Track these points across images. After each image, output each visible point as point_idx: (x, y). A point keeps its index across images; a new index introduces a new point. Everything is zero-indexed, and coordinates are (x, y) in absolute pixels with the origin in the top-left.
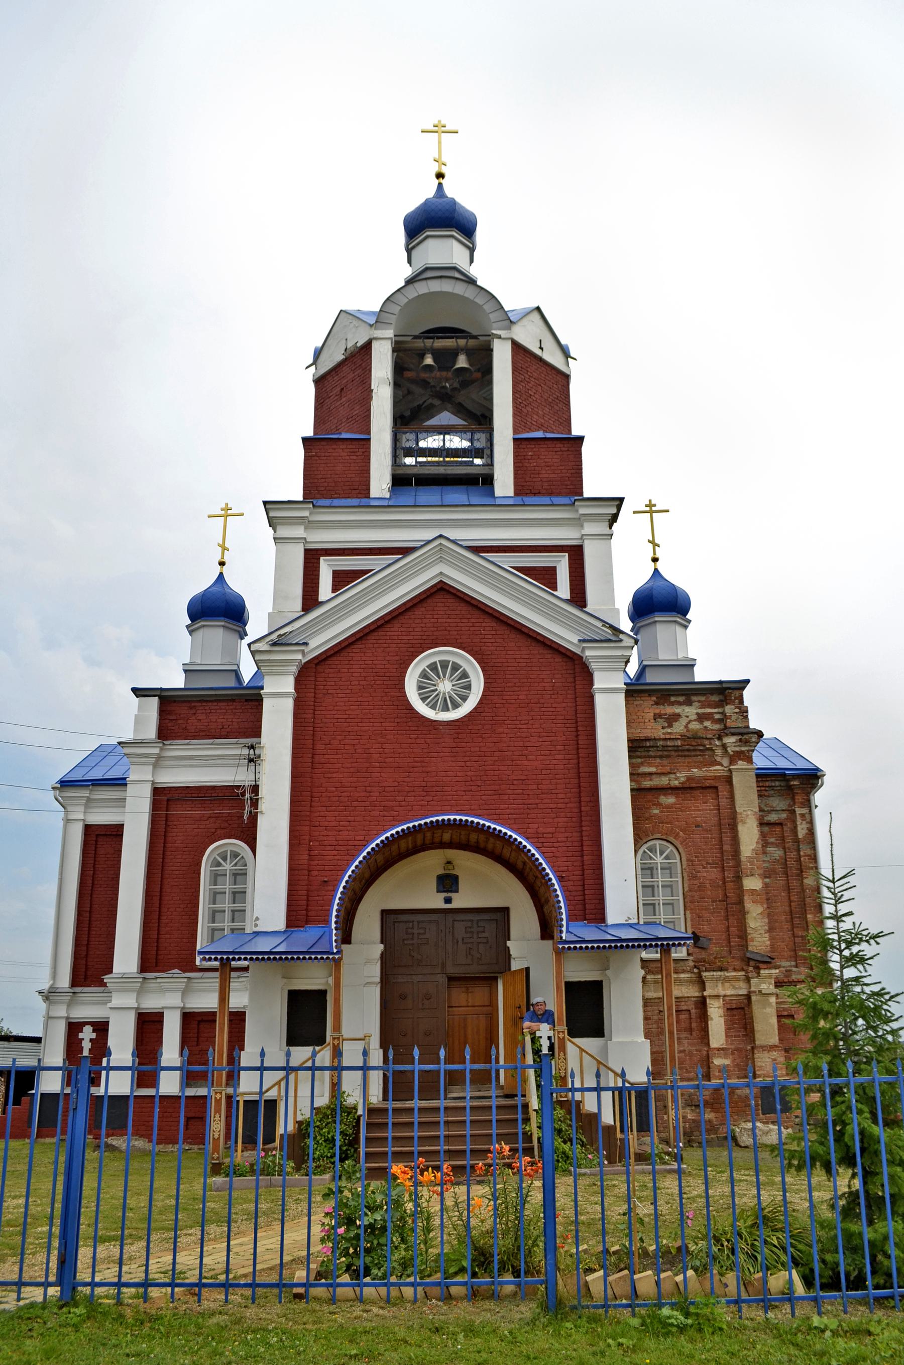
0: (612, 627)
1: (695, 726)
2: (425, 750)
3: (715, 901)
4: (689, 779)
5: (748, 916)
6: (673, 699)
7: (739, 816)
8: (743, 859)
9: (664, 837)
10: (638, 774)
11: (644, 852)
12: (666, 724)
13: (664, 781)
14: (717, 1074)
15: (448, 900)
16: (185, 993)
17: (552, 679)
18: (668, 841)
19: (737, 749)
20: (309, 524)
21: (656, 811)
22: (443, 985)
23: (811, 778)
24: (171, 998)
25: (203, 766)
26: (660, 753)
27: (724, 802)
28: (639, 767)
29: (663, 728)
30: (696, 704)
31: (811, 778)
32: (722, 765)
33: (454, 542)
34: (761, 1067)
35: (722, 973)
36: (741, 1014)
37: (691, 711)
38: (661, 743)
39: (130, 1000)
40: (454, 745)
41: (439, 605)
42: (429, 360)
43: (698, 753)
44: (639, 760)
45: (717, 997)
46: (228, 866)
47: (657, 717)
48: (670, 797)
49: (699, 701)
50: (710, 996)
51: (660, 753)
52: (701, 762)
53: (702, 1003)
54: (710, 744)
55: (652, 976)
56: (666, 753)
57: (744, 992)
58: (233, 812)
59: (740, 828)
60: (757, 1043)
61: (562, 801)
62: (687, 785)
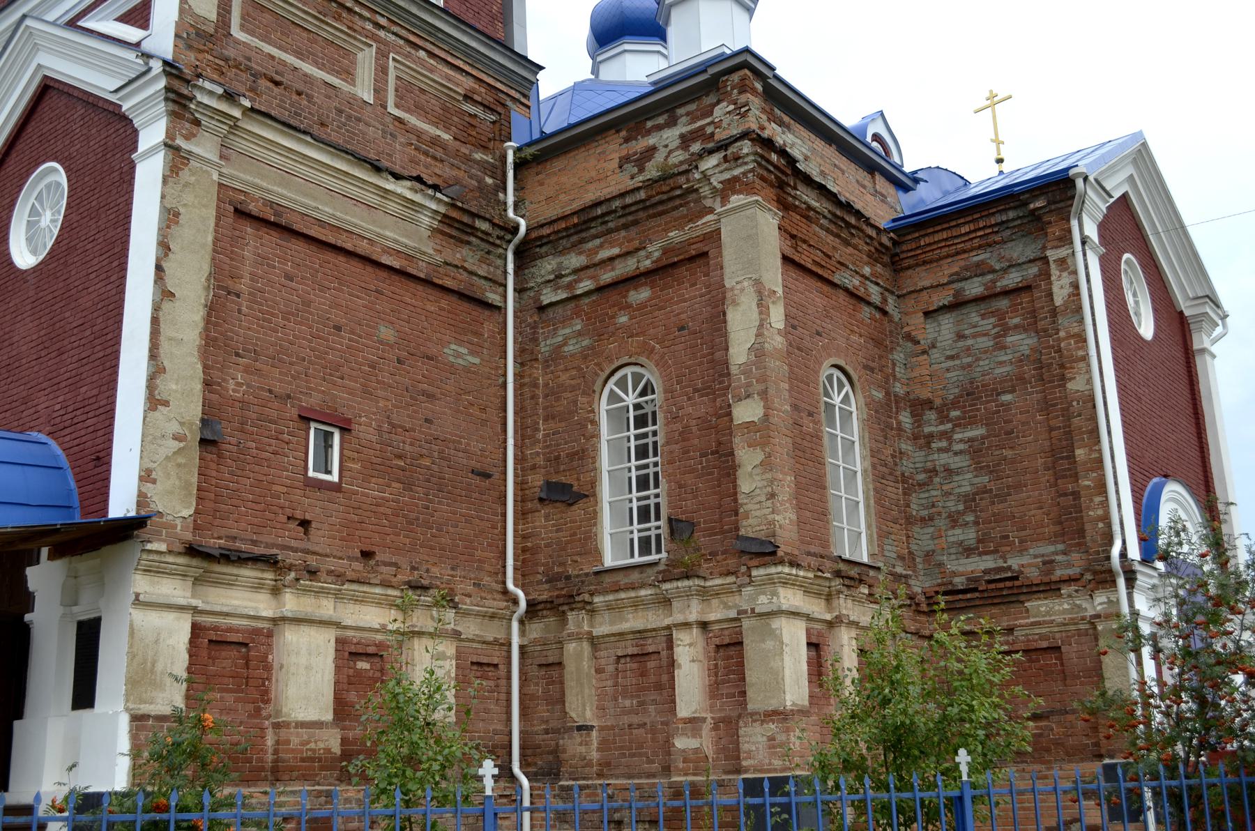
4: (666, 251)
5: (740, 473)
6: (649, 124)
7: (729, 295)
8: (734, 370)
10: (595, 265)
11: (612, 390)
13: (629, 266)
14: (681, 765)
19: (727, 176)
21: (623, 319)
28: (597, 253)
34: (749, 752)
36: (729, 653)
37: (671, 136)
43: (678, 202)
44: (597, 242)
45: (686, 625)
48: (642, 289)
49: (688, 114)
50: (675, 625)
51: (623, 221)
54: (688, 181)
56: (630, 218)
57: (732, 614)
60: (750, 707)
62: (664, 262)
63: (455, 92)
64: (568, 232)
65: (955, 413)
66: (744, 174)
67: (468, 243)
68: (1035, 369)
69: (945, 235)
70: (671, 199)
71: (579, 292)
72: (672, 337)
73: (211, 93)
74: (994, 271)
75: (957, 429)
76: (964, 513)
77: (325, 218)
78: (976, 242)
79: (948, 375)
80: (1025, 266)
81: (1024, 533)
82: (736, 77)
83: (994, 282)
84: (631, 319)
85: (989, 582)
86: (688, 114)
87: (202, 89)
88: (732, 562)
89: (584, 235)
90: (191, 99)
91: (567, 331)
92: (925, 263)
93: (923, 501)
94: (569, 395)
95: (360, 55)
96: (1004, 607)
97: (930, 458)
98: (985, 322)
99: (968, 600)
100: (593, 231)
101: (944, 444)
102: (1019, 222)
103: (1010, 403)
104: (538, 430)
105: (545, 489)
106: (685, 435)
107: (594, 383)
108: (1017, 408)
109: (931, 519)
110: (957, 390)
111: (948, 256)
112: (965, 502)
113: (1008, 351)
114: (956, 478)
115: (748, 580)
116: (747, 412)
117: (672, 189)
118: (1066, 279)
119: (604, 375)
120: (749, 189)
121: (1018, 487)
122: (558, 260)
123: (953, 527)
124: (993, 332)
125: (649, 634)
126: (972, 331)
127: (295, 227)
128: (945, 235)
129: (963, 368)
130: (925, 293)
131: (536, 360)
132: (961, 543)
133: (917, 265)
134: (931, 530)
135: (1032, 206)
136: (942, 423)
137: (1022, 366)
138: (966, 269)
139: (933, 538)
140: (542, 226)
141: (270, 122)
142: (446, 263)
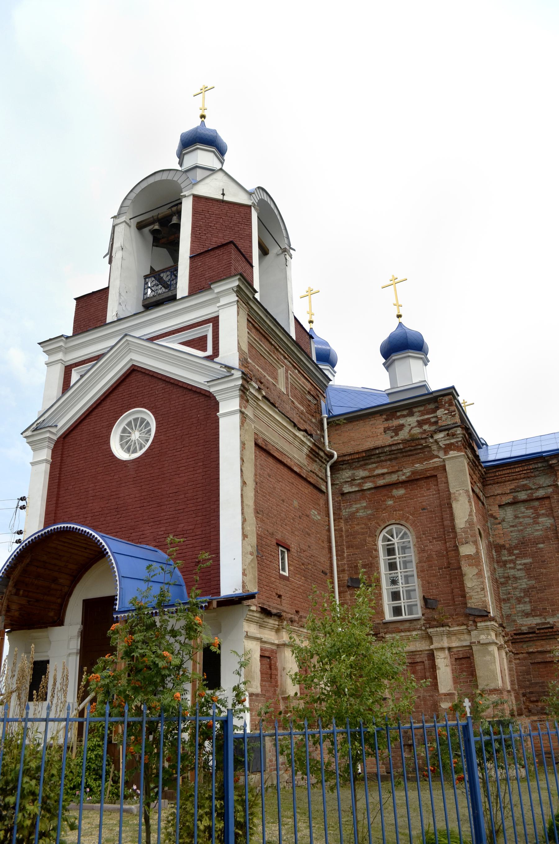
0: (226, 367)
1: (416, 431)
2: (118, 483)
3: (442, 569)
4: (413, 473)
6: (398, 414)
7: (452, 496)
8: (458, 531)
9: (397, 522)
10: (374, 476)
12: (393, 434)
13: (394, 478)
17: (197, 415)
18: (402, 525)
19: (448, 442)
26: (389, 457)
28: (374, 471)
29: (392, 437)
30: (417, 414)
32: (439, 457)
33: (139, 338)
35: (444, 629)
36: (465, 662)
37: (412, 420)
38: (387, 449)
40: (136, 475)
41: (132, 381)
43: (419, 451)
44: (374, 465)
45: (442, 649)
49: (419, 411)
50: (436, 649)
51: (389, 457)
52: (422, 458)
53: (431, 656)
54: (426, 442)
55: (390, 635)
56: (393, 456)
57: (467, 643)
59: (454, 505)
61: (200, 503)
62: (413, 478)
63: (304, 388)
64: (359, 460)
65: (516, 552)
66: (457, 442)
67: (316, 461)
68: (553, 534)
69: (508, 471)
70: (415, 450)
71: (365, 488)
72: (419, 512)
73: (254, 387)
74: (531, 489)
75: (518, 559)
76: (524, 597)
77: (279, 448)
78: (522, 476)
79: (512, 534)
80: (546, 488)
81: (553, 607)
82: (447, 398)
83: (532, 494)
84: (394, 502)
85: (538, 629)
86: (419, 411)
87: (252, 385)
88: (461, 619)
89: (367, 461)
90: (247, 390)
91: (358, 506)
92: (498, 483)
93: (504, 591)
94: (361, 536)
95: (279, 371)
96: (547, 641)
97: (506, 571)
98: (528, 511)
99: (530, 637)
100: (372, 460)
101: (512, 565)
102: (543, 468)
103: (543, 548)
104: (344, 552)
105: (350, 581)
106: (429, 559)
107: (375, 531)
108: (546, 550)
109: (508, 599)
110: (516, 541)
111: (509, 481)
112: (524, 592)
113: (540, 525)
114: (519, 581)
115: (475, 628)
116: (466, 550)
117: (417, 445)
119: (380, 528)
120: (458, 449)
121: (550, 586)
122: (353, 472)
123: (519, 604)
124: (532, 516)
125: (417, 653)
126: (522, 515)
127: (271, 452)
128: (508, 471)
129: (519, 531)
130: (499, 497)
131: (341, 518)
132: (523, 611)
133: (494, 484)
134: (509, 605)
135: (551, 462)
136: (510, 556)
137: (547, 532)
138: (518, 487)
139: (510, 609)
140: (345, 456)
141: (267, 402)
142: (311, 471)
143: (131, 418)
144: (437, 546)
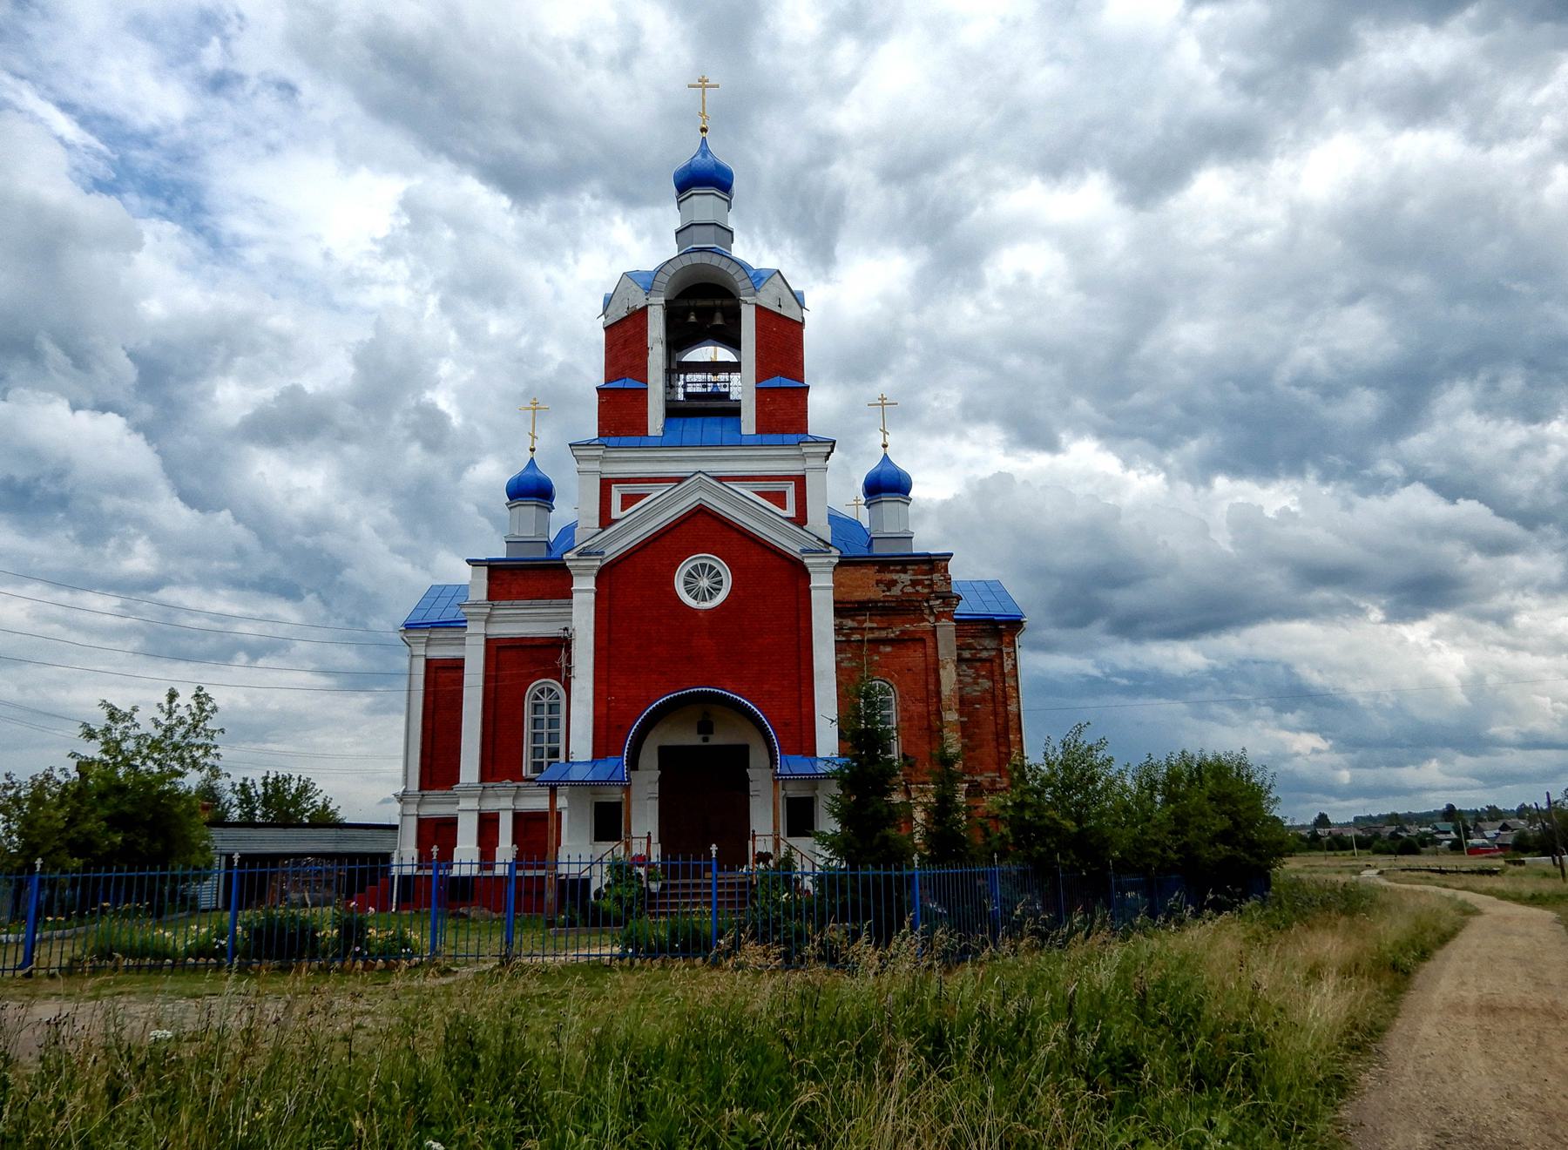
1: (909, 590)
4: (903, 632)
13: (883, 634)
15: (706, 740)
16: (515, 798)
20: (603, 460)
22: (704, 802)
23: (1014, 625)
24: (504, 804)
25: (525, 622)
27: (930, 651)
31: (1014, 625)
37: (905, 578)
39: (473, 804)
42: (692, 318)
46: (545, 700)
47: (878, 582)
58: (549, 655)
106: (910, 719)
118: (1010, 662)
143: (698, 562)
144: (920, 708)
